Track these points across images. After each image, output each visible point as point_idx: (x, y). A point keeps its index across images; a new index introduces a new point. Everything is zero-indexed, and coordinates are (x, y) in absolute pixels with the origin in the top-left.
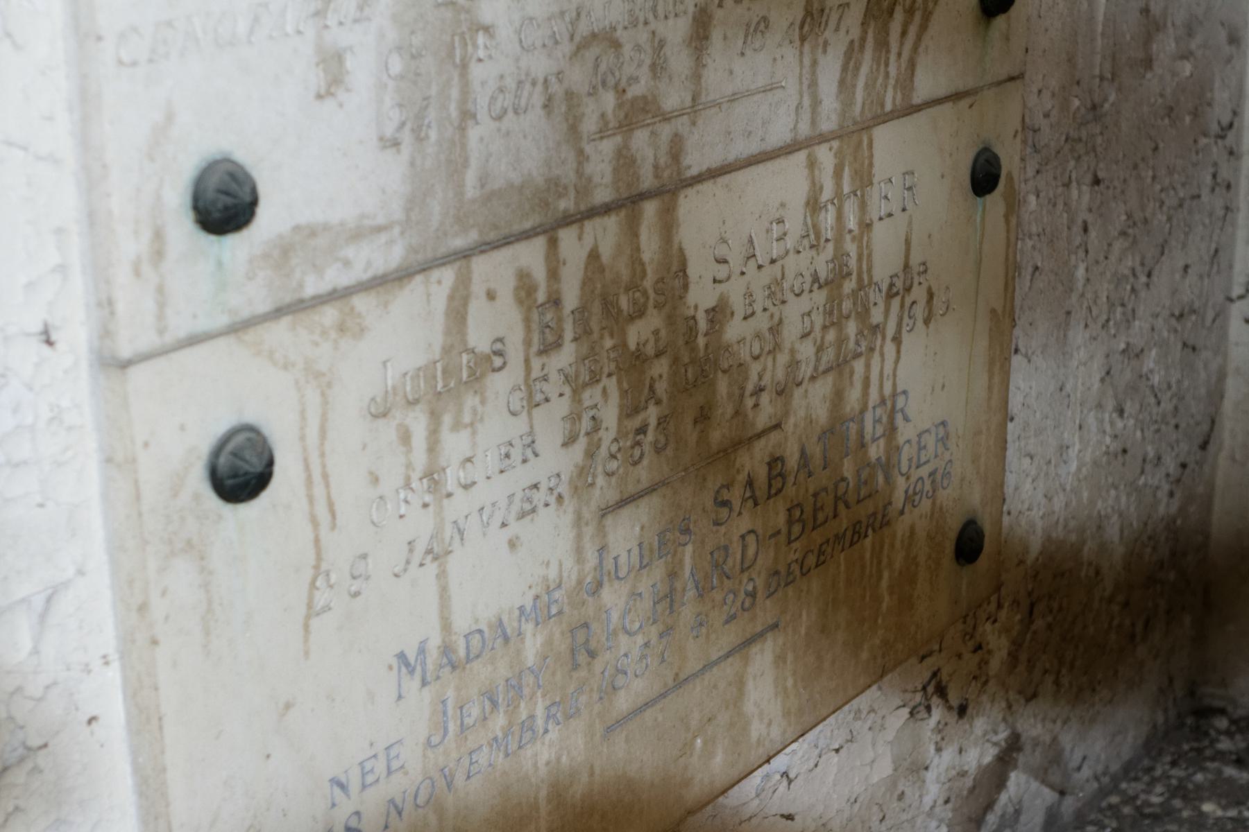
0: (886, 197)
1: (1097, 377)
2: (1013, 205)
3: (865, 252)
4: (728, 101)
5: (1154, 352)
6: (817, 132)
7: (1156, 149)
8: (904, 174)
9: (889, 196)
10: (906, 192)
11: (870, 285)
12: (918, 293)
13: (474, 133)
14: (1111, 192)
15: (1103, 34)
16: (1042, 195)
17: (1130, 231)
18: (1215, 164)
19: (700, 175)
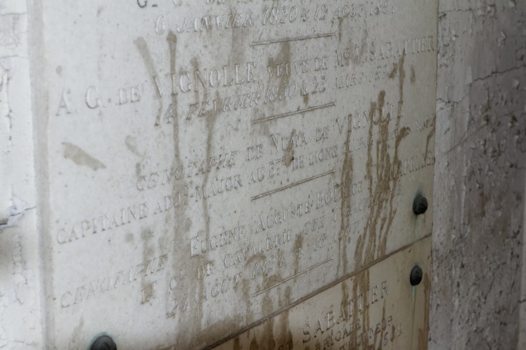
0: (375, 294)
1: (464, 343)
2: (428, 287)
3: (366, 318)
4: (310, 270)
5: (488, 329)
6: (346, 274)
7: (487, 248)
8: (382, 283)
9: (376, 293)
10: (383, 290)
11: (368, 330)
12: (389, 329)
13: (205, 304)
14: (469, 268)
15: (464, 207)
16: (440, 275)
17: (477, 282)
18: (512, 249)
19: (298, 301)
